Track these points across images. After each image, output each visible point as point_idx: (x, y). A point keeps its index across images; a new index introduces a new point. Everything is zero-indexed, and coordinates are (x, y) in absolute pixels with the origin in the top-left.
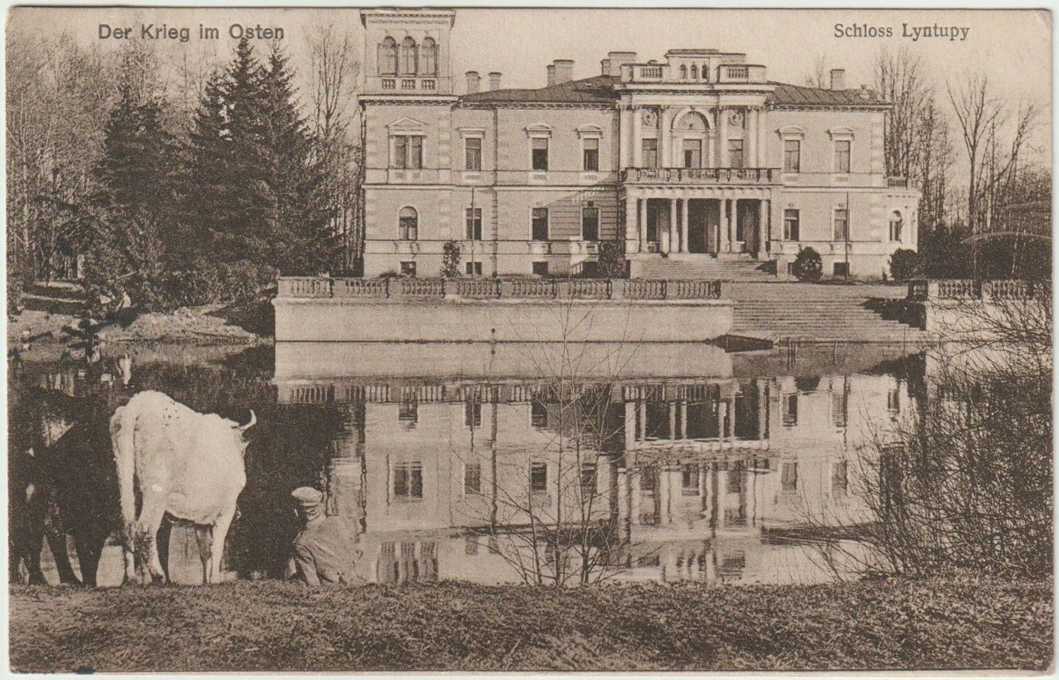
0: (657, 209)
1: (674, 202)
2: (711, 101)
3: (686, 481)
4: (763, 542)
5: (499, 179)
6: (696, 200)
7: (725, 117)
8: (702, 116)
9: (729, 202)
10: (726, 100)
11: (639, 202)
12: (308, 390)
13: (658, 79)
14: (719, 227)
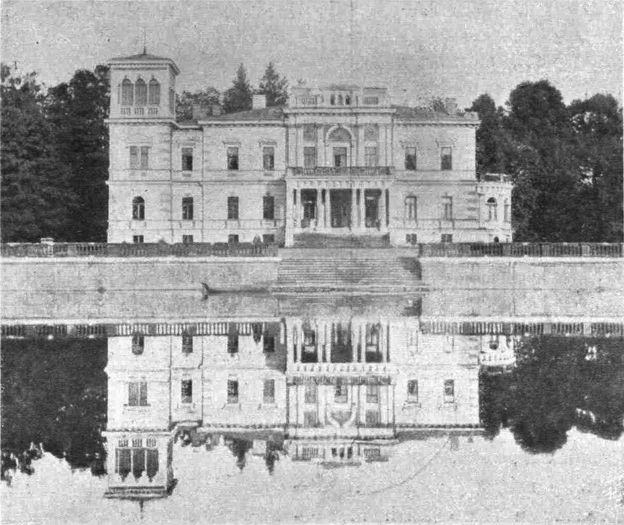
0: (309, 196)
1: (320, 192)
2: (352, 120)
3: (338, 393)
4: (492, 439)
5: (173, 177)
6: (340, 191)
7: (361, 132)
8: (346, 130)
9: (324, 192)
10: (362, 120)
11: (295, 191)
12: (579, 325)
13: (314, 106)
14: (285, 208)
